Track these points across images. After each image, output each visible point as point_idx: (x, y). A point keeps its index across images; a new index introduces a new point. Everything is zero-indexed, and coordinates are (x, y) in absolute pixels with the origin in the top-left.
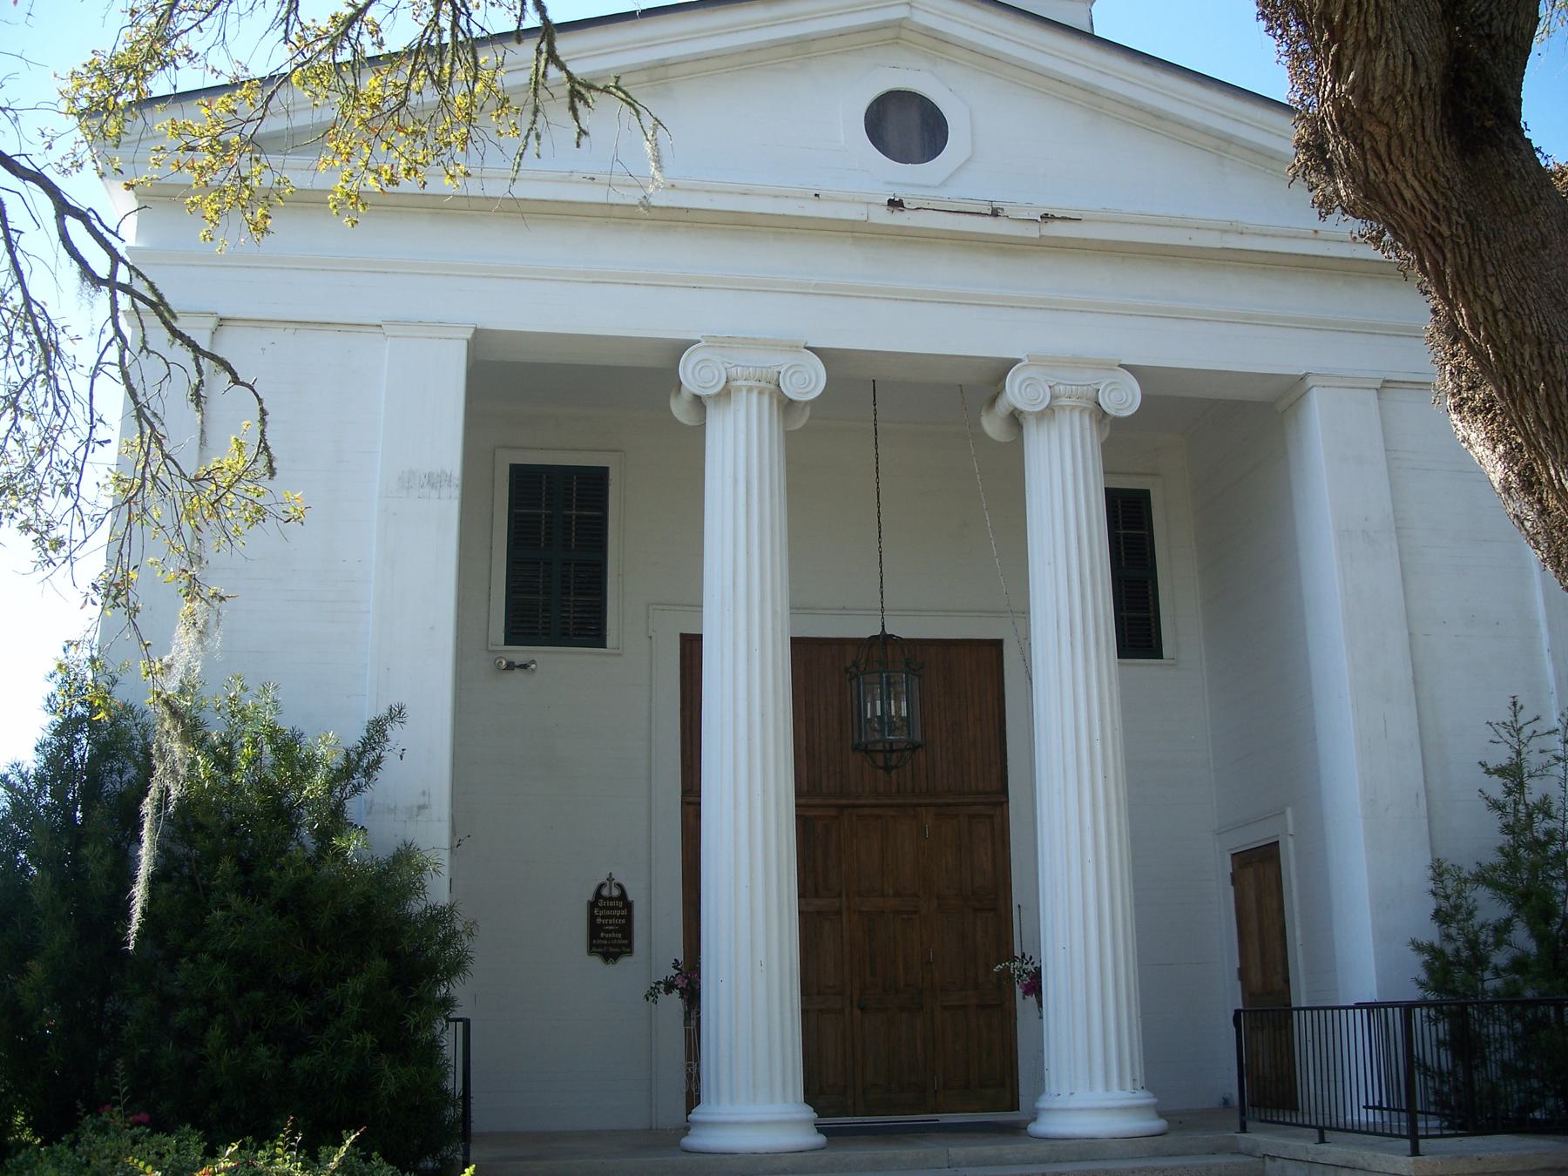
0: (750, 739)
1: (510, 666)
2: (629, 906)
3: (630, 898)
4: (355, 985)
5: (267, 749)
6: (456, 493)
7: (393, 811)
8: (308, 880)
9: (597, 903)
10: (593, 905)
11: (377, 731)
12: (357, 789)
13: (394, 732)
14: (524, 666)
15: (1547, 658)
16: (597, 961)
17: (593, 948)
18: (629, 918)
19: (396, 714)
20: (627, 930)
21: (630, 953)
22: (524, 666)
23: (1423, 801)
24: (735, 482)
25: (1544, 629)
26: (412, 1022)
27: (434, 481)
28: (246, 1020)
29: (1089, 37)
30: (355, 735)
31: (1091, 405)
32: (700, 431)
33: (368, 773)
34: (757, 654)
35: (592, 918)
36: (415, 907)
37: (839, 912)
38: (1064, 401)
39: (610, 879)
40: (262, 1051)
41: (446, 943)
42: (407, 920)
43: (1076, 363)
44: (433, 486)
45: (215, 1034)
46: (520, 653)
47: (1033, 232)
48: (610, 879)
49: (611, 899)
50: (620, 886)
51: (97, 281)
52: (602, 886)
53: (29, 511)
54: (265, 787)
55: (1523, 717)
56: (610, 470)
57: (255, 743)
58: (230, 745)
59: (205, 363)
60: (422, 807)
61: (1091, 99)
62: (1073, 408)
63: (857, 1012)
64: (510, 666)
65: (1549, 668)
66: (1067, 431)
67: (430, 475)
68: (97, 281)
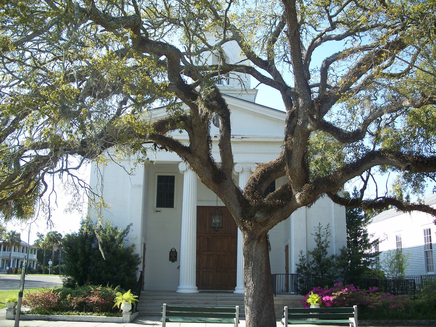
0: (188, 228)
1: (157, 211)
2: (176, 253)
3: (177, 251)
4: (122, 266)
5: (111, 231)
6: (142, 188)
7: (131, 239)
8: (116, 250)
9: (171, 252)
10: (170, 252)
11: (129, 227)
12: (125, 236)
13: (131, 227)
14: (159, 211)
15: (333, 214)
16: (171, 262)
17: (170, 260)
18: (176, 255)
19: (131, 224)
20: (176, 257)
21: (176, 261)
22: (159, 211)
23: (306, 239)
24: (187, 185)
25: (333, 209)
26: (131, 271)
27: (139, 186)
28: (404, 277)
29: (254, 103)
30: (125, 228)
31: (250, 170)
32: (183, 175)
33: (127, 234)
34: (190, 214)
35: (170, 255)
36: (133, 254)
37: (213, 255)
38: (245, 170)
39: (173, 248)
40: (109, 275)
41: (138, 260)
42: (131, 256)
43: (247, 163)
44: (138, 187)
45: (103, 272)
46: (159, 209)
47: (240, 140)
48: (173, 248)
49: (173, 251)
50: (175, 249)
51: (83, 187)
52: (172, 249)
53: (77, 207)
54: (111, 236)
55: (321, 226)
56: (175, 177)
57: (109, 230)
58: (106, 230)
59: (95, 195)
60: (136, 238)
61: (255, 114)
62: (246, 171)
63: (216, 272)
64: (157, 211)
65: (333, 216)
66: (245, 175)
67: (138, 185)
68: (83, 187)
